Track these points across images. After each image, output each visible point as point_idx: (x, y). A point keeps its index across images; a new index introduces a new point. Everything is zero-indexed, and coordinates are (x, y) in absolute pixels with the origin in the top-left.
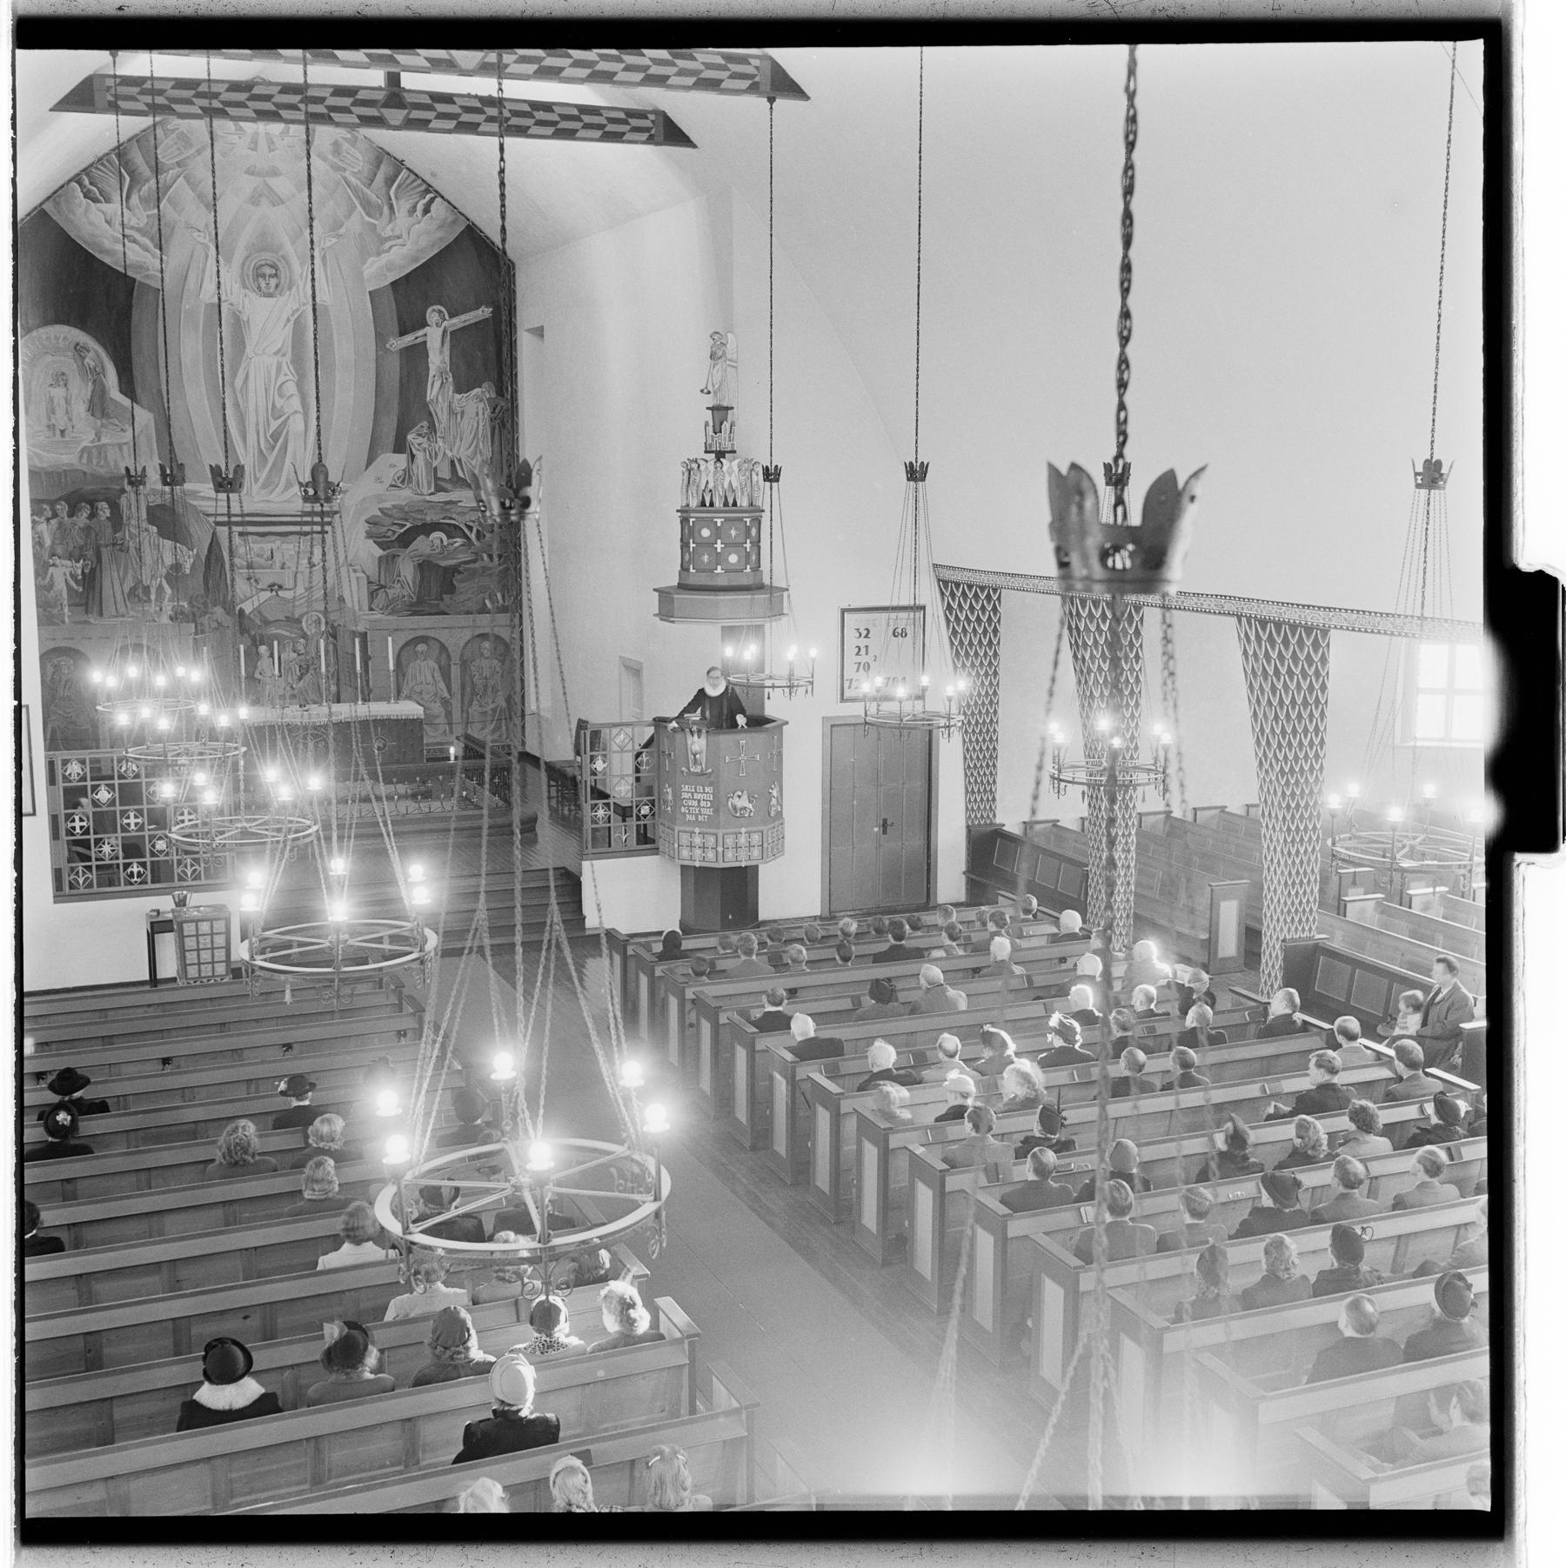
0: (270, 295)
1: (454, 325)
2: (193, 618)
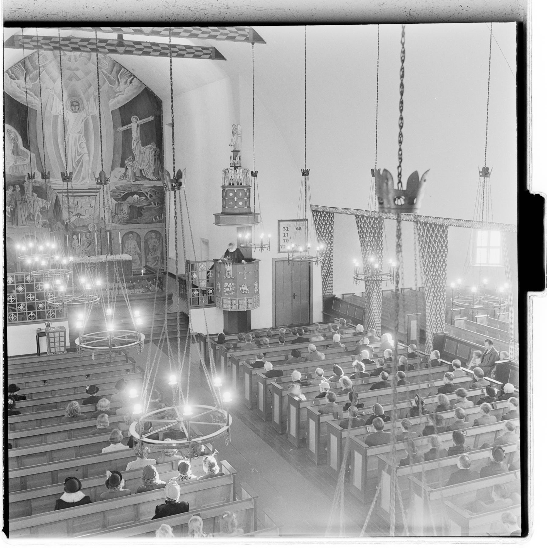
0: (76, 112)
1: (141, 122)
2: (50, 226)
